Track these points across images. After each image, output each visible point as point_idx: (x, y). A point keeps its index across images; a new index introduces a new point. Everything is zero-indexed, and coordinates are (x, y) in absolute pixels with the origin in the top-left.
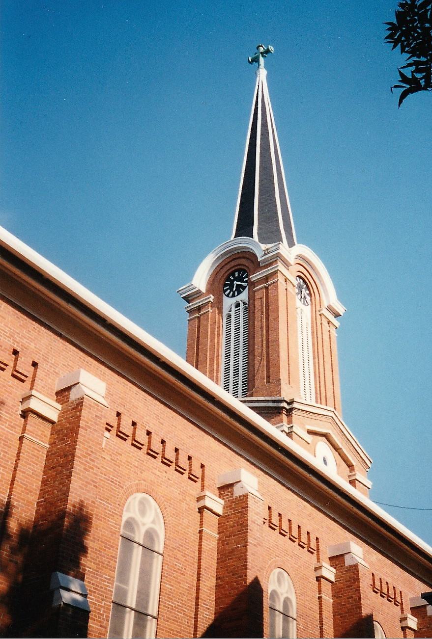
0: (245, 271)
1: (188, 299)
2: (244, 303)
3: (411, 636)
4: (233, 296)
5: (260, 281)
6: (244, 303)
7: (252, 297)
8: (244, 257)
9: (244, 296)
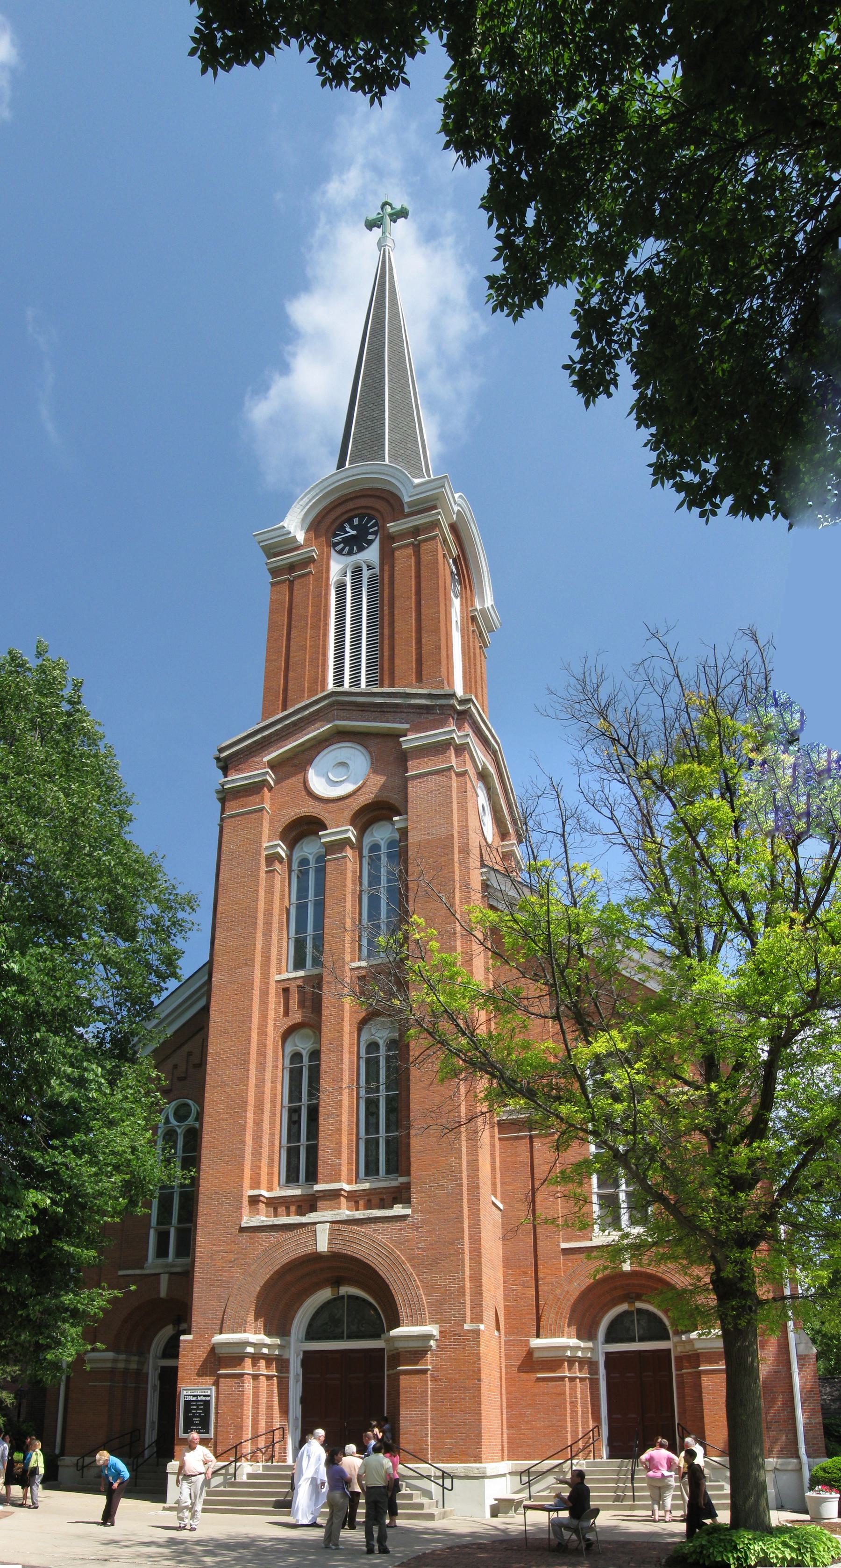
0: (371, 518)
1: (271, 551)
2: (370, 567)
3: (840, 381)
4: (350, 553)
5: (402, 535)
6: (370, 567)
7: (387, 555)
8: (388, 501)
9: (372, 554)
